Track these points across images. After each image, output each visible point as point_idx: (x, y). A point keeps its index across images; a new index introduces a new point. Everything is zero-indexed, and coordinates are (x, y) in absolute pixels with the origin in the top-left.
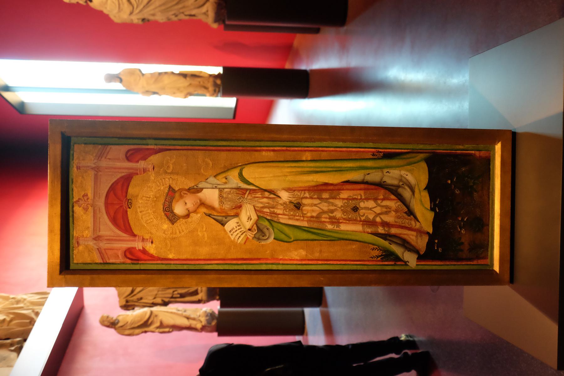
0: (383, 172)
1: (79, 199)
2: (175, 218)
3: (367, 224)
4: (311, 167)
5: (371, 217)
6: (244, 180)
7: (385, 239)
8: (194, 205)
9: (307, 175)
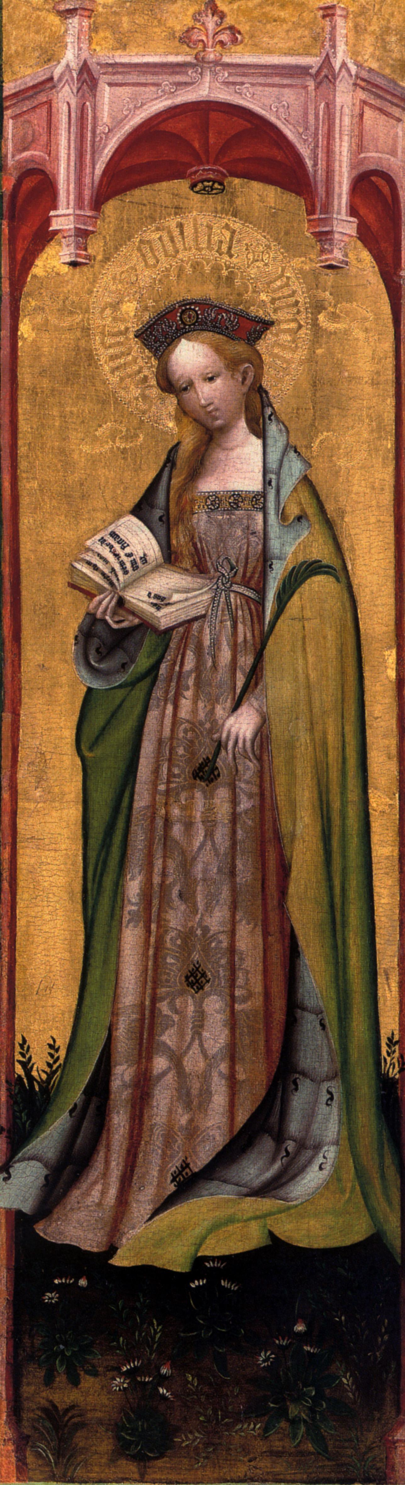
0: (329, 1078)
1: (222, 16)
2: (158, 344)
3: (142, 1020)
4: (344, 817)
5: (168, 1038)
6: (296, 581)
7: (90, 1091)
8: (205, 407)
9: (317, 803)
